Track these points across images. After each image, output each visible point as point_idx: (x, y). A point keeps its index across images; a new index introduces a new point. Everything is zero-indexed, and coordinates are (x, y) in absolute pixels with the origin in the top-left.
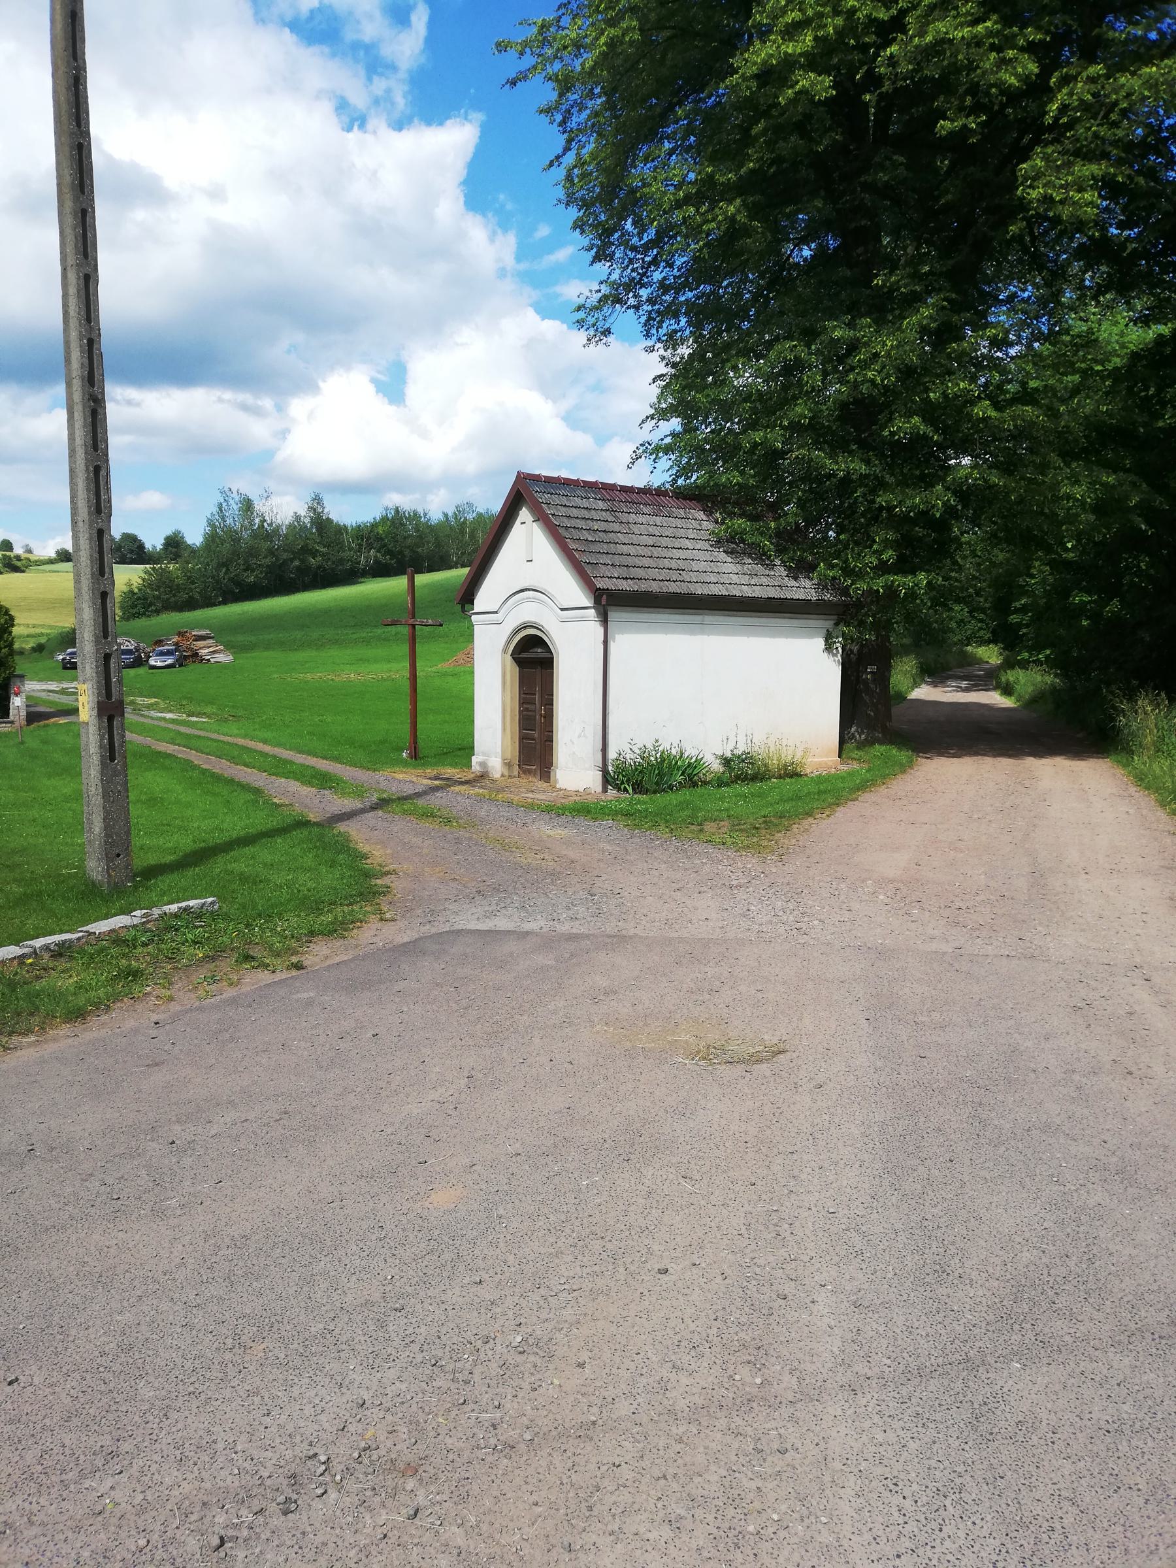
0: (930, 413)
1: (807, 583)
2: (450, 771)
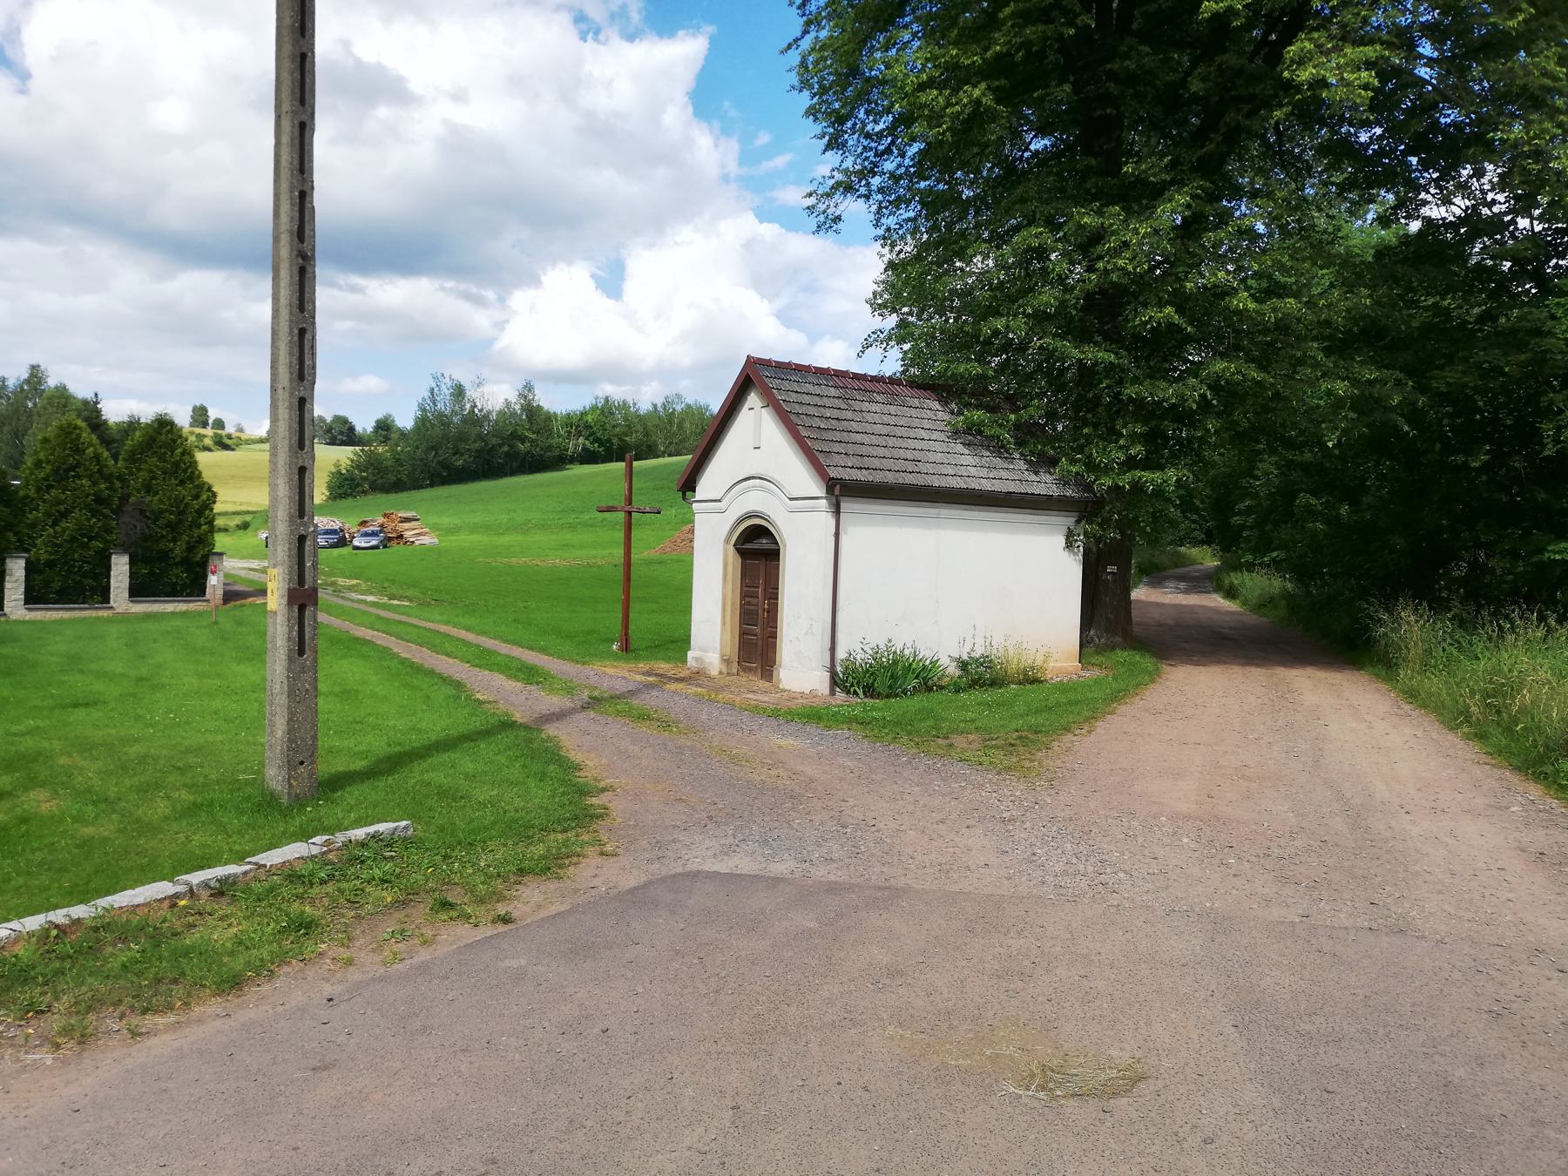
0: (1181, 302)
1: (1048, 478)
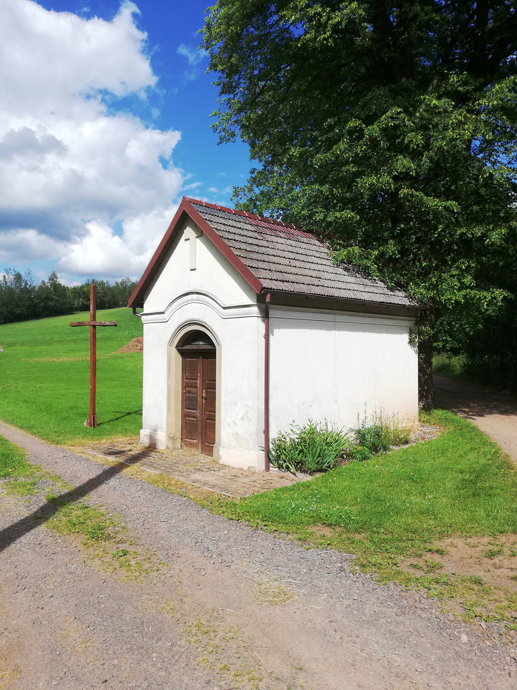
2: (121, 441)
